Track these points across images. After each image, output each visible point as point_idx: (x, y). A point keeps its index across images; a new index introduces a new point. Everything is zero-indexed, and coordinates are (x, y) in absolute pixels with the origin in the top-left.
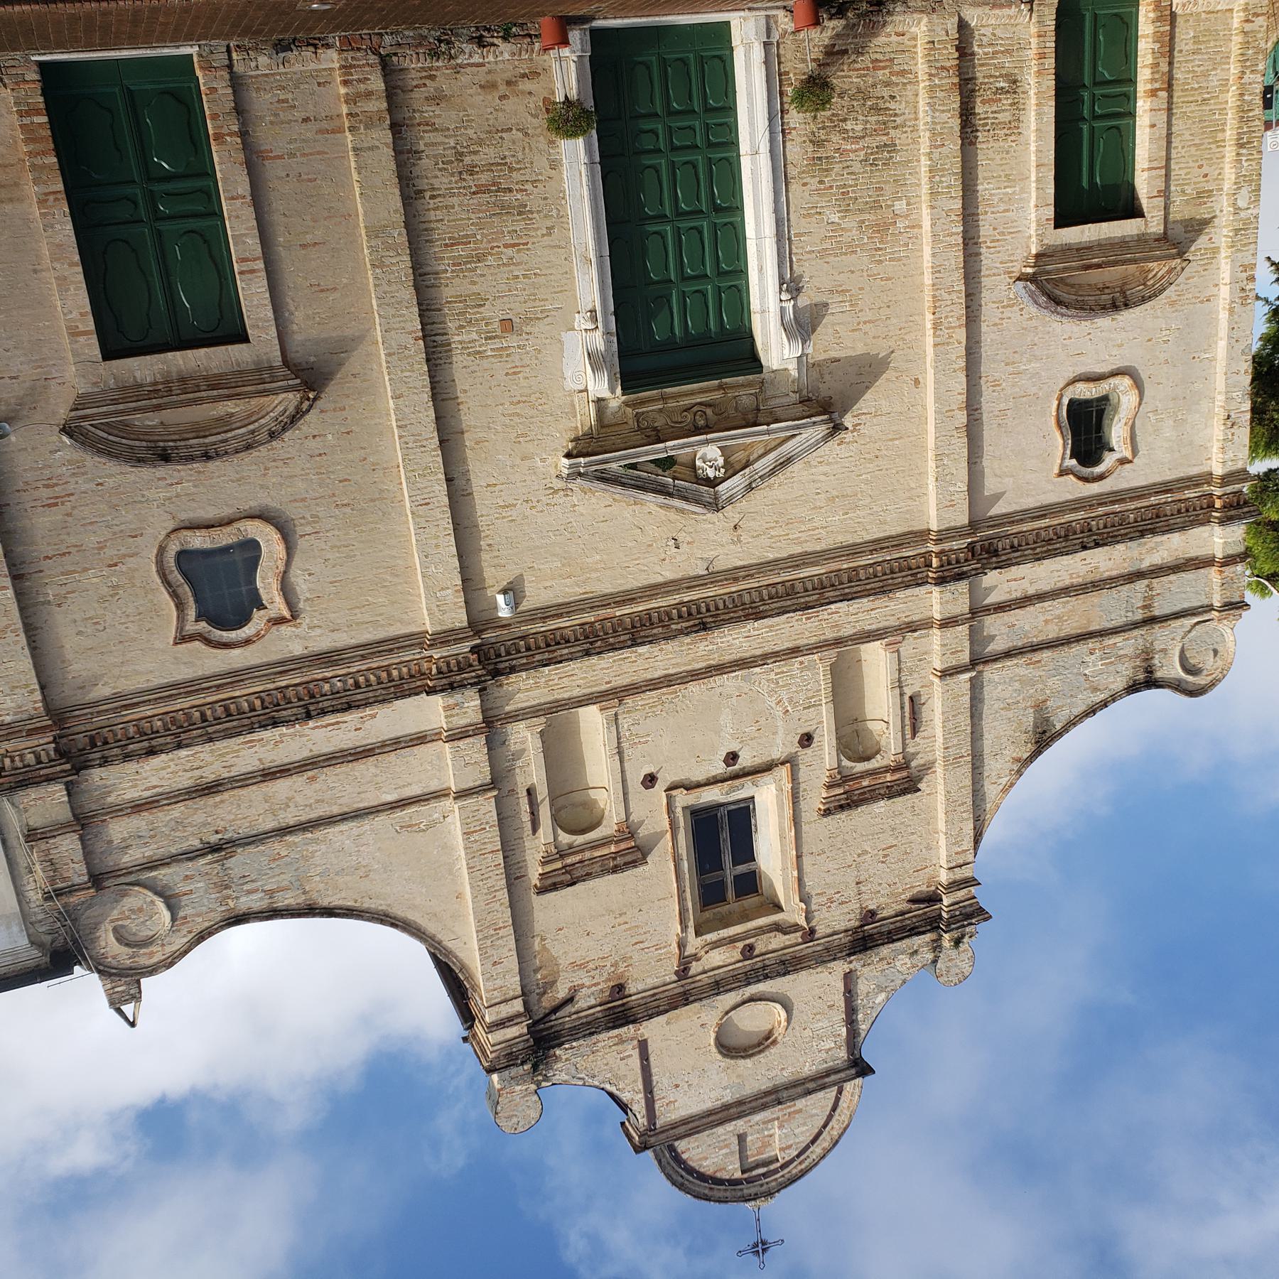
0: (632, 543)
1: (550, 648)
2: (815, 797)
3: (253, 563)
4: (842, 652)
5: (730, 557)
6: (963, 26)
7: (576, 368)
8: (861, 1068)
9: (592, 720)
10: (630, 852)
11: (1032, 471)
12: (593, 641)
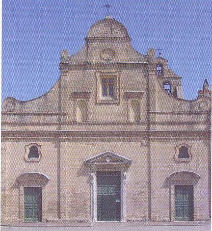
0: (125, 150)
1: (137, 134)
2: (92, 97)
3: (179, 155)
4: (85, 122)
5: (105, 143)
6: (60, 218)
7: (128, 178)
8: (86, 39)
9: (132, 120)
10: (127, 95)
11: (47, 148)
12: (131, 134)
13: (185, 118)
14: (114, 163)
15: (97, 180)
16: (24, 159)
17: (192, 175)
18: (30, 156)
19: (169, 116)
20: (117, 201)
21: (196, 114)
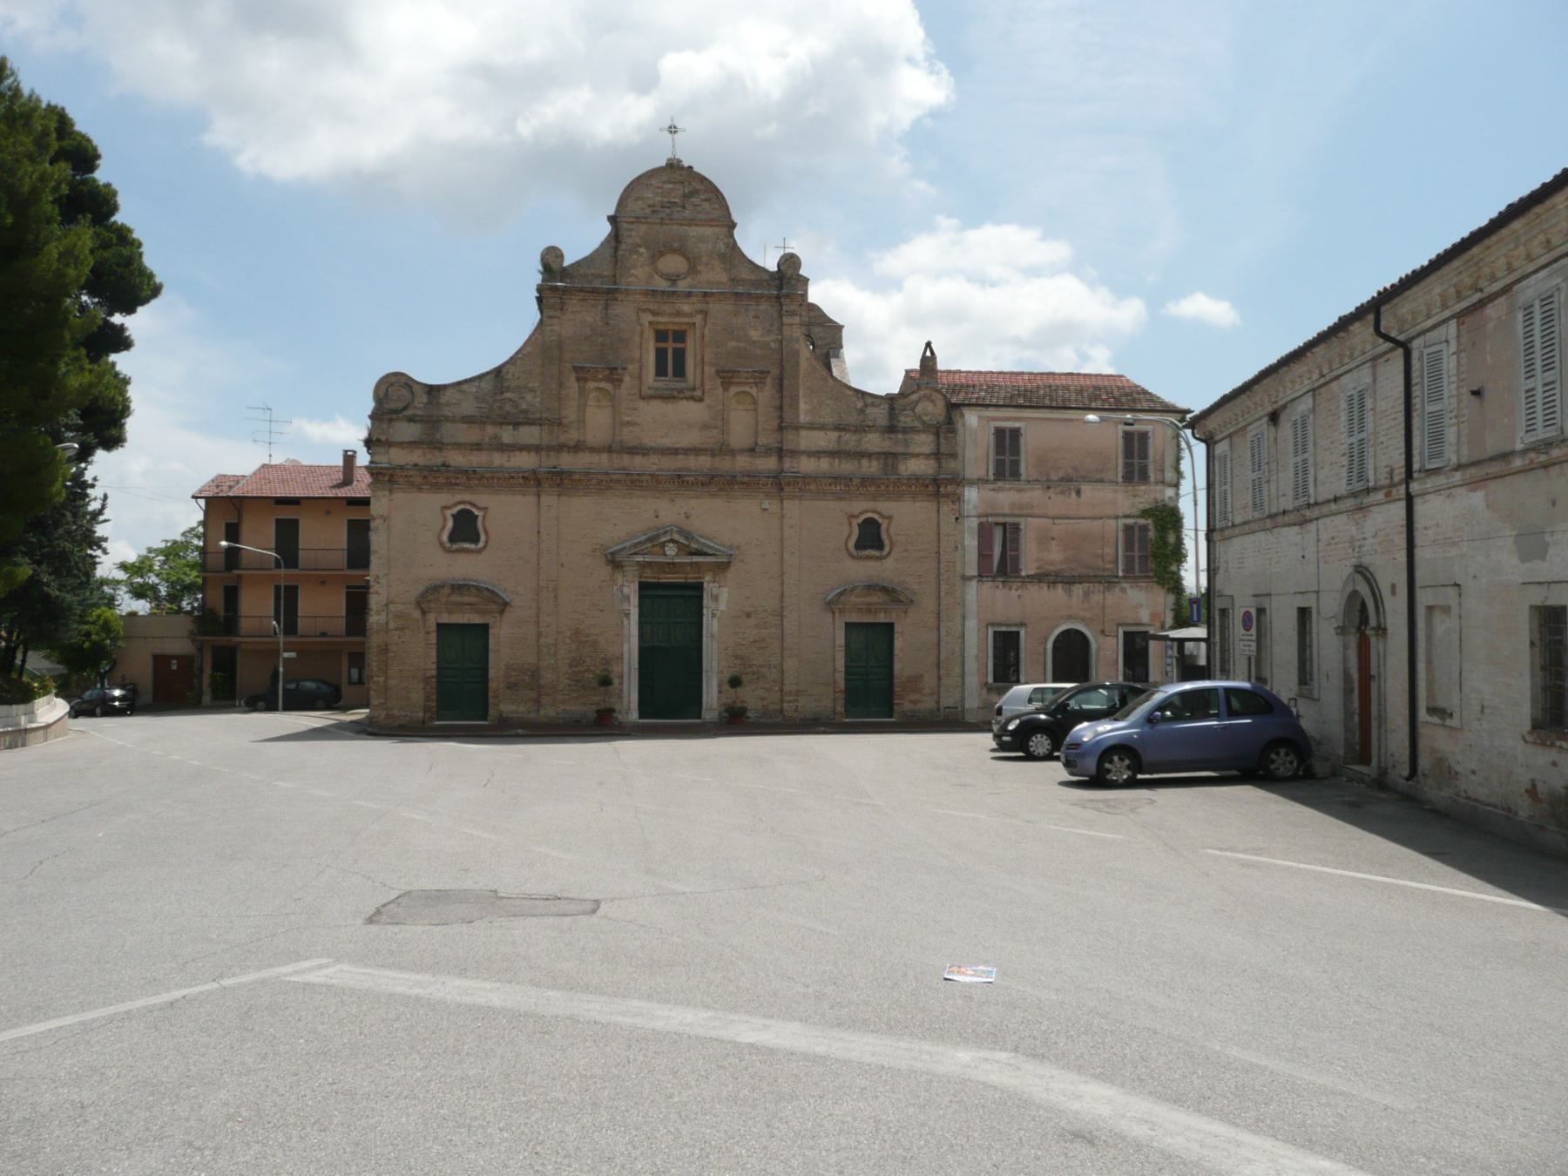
0: (715, 520)
13: (874, 442)
14: (687, 559)
15: (641, 606)
16: (442, 544)
17: (891, 593)
18: (452, 539)
19: (833, 435)
20: (98, 711)
21: (905, 431)
